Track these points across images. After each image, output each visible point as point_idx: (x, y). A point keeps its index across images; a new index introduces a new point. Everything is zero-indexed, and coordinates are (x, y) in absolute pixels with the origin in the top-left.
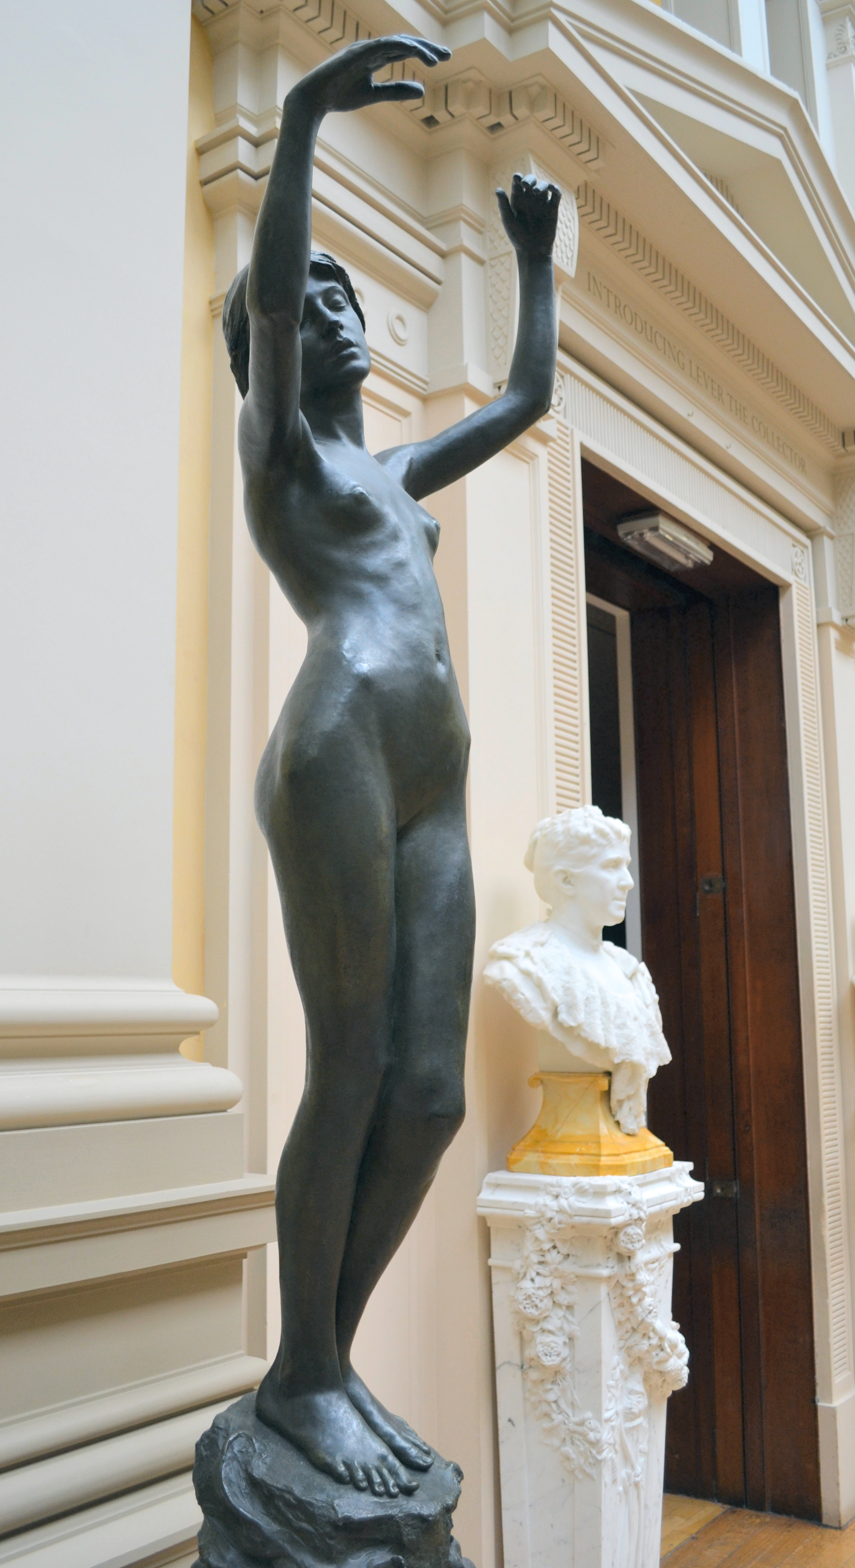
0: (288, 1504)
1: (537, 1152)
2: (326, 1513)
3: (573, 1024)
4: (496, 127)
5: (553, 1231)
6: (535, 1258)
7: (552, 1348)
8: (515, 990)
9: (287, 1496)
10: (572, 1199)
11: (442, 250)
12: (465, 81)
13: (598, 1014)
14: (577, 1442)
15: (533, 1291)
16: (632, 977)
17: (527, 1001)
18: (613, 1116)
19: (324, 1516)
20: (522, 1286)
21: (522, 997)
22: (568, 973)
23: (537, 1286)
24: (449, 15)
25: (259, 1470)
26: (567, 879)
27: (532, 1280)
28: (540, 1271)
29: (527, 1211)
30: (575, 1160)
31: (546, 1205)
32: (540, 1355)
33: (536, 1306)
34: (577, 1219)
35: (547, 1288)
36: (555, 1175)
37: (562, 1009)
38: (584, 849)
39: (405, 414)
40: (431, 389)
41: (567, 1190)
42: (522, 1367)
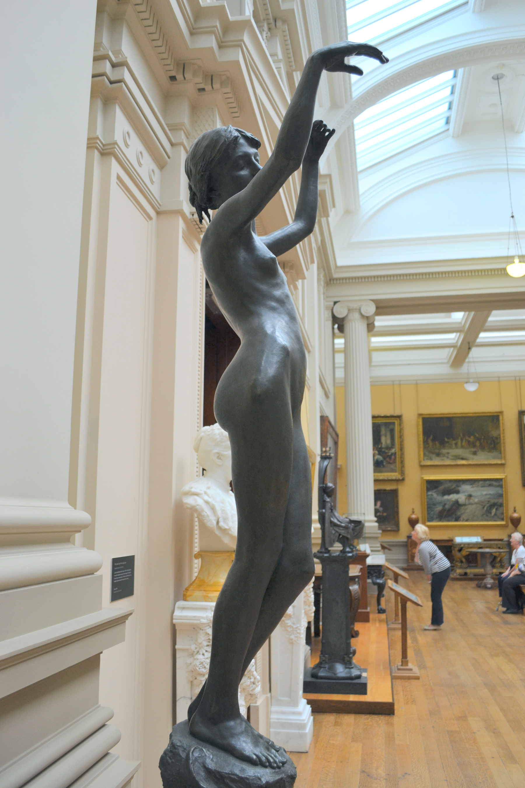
0: (233, 780)
2: (255, 782)
3: (227, 527)
8: (203, 510)
9: (232, 776)
12: (194, 64)
17: (208, 516)
19: (255, 784)
22: (223, 503)
24: (194, 31)
25: (211, 765)
27: (203, 654)
29: (202, 620)
33: (205, 667)
37: (221, 520)
39: (150, 218)
40: (162, 209)
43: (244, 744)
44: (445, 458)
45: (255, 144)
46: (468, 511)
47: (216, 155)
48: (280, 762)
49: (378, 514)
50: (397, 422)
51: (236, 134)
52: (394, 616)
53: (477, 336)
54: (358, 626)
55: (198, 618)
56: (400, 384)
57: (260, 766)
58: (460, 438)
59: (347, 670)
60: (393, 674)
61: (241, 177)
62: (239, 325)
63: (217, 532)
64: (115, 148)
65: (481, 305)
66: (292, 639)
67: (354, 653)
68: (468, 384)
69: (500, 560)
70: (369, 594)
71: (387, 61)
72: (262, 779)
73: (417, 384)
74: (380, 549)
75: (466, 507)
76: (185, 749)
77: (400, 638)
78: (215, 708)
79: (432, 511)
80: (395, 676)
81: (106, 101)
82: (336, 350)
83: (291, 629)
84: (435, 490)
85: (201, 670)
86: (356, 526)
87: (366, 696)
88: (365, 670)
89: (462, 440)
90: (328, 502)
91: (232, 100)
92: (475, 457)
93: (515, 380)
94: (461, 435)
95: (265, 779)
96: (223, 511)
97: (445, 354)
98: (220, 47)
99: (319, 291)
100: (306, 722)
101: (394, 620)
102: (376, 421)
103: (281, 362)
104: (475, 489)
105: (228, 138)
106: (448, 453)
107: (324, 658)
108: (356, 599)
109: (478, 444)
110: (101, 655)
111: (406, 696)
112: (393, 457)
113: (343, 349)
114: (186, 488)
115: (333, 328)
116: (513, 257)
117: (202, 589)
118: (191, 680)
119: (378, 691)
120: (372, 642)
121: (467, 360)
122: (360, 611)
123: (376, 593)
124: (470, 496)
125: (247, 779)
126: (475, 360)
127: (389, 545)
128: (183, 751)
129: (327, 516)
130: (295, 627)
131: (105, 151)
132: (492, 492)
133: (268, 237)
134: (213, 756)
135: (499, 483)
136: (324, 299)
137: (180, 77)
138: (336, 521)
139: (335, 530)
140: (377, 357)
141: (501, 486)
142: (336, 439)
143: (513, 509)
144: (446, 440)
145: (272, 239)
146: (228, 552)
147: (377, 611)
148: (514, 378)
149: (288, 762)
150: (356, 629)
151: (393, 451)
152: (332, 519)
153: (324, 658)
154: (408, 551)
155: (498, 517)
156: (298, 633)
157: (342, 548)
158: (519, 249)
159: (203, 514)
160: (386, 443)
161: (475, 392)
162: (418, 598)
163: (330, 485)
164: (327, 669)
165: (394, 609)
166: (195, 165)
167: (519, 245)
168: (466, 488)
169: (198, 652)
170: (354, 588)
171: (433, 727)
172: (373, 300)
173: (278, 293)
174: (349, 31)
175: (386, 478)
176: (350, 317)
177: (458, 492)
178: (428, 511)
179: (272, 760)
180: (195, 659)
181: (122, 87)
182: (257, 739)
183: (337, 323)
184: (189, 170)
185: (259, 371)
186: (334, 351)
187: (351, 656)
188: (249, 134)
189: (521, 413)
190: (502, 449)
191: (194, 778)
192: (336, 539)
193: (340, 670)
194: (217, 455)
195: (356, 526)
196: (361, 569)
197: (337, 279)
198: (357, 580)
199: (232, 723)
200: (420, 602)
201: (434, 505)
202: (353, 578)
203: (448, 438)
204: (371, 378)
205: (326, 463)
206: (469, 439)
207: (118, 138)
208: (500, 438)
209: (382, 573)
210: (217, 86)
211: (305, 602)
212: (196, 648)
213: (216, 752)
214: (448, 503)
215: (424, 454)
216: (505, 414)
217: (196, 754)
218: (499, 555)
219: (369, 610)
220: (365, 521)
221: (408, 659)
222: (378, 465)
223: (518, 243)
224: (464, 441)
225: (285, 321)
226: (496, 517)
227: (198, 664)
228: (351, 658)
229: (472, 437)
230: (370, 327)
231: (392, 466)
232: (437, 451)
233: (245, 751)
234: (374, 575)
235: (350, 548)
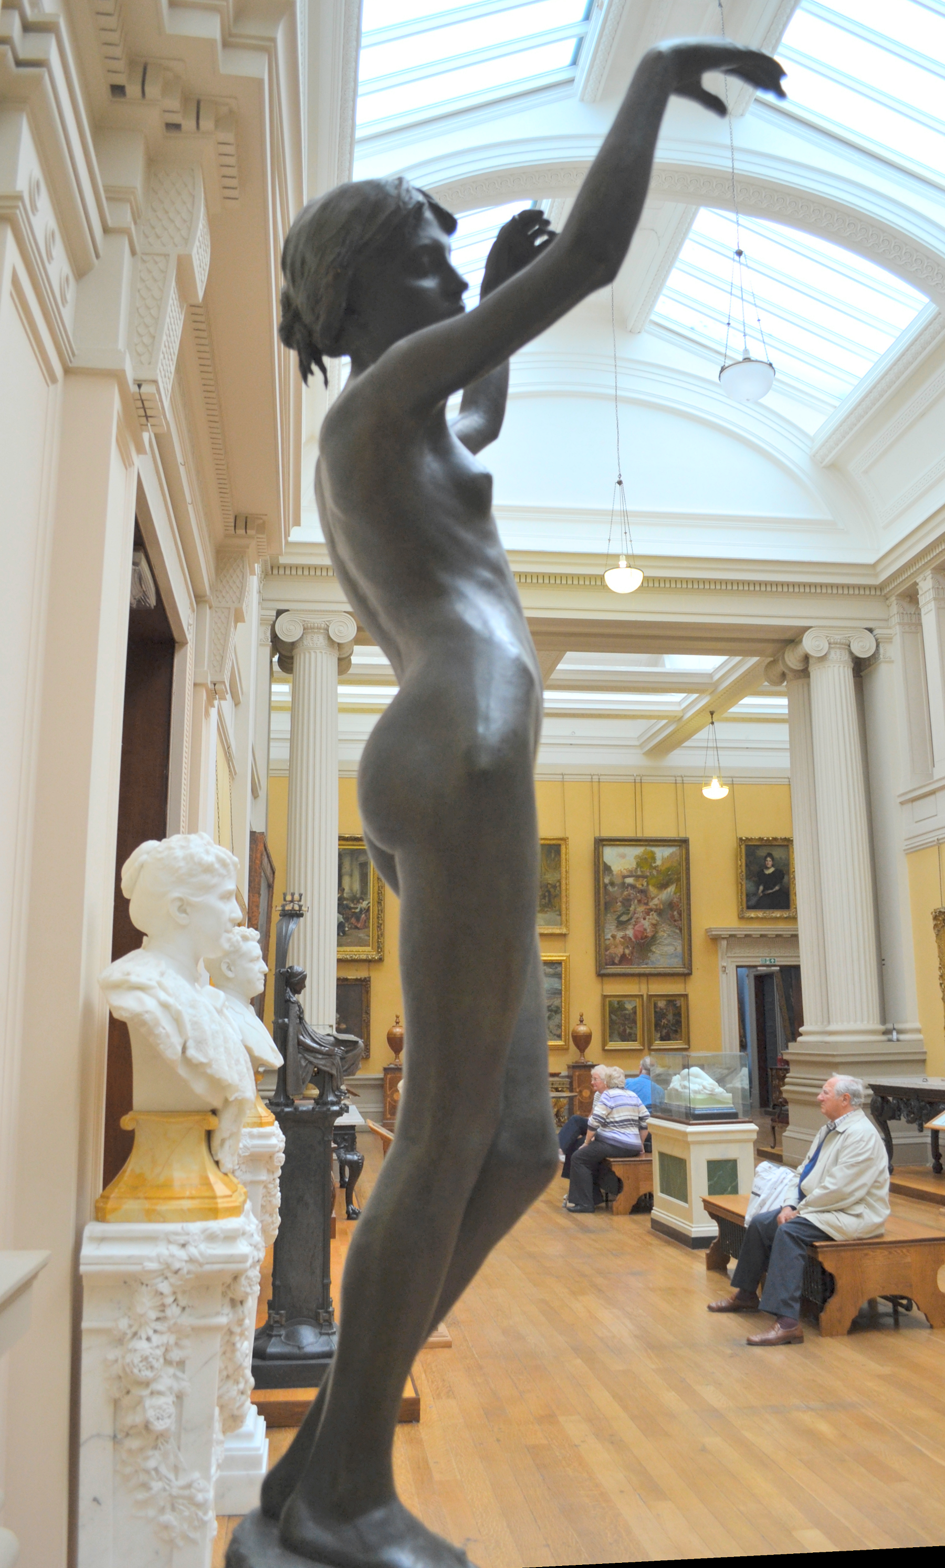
1: (139, 1198)
3: (203, 1060)
4: (174, 127)
5: (180, 1283)
6: (153, 1315)
7: (164, 1411)
8: (157, 1024)
10: (203, 1247)
13: (222, 1050)
14: (181, 1507)
17: (168, 1036)
18: (212, 1155)
21: (163, 1031)
26: (183, 906)
27: (148, 1339)
31: (173, 1256)
32: (152, 1419)
33: (152, 1367)
34: (208, 1267)
35: (162, 1345)
36: (164, 1222)
37: (190, 1044)
38: (206, 878)
39: (54, 380)
41: (196, 1237)
42: (115, 1437)
51: (421, 198)
55: (139, 1260)
59: (324, 1338)
61: (424, 291)
63: (182, 1071)
64: (17, 207)
85: (143, 1373)
86: (347, 1052)
96: (195, 1024)
98: (225, 45)
105: (404, 203)
107: (277, 1317)
115: (271, 662)
116: (617, 556)
118: (117, 1396)
129: (291, 1030)
137: (133, 90)
138: (308, 1041)
139: (306, 1059)
141: (559, 976)
146: (198, 1112)
147: (346, 1216)
151: (364, 904)
152: (301, 1037)
153: (277, 1317)
154: (385, 1096)
158: (629, 543)
159: (156, 1032)
160: (351, 889)
169: (135, 1334)
171: (498, 1440)
174: (361, 90)
176: (307, 642)
180: (130, 1351)
189: (601, 843)
190: (564, 906)
194: (178, 904)
195: (347, 1052)
208: (560, 886)
210: (207, 124)
211: (262, 1206)
212: (130, 1326)
216: (570, 842)
227: (136, 1361)
230: (344, 664)
231: (361, 935)
235: (336, 1096)
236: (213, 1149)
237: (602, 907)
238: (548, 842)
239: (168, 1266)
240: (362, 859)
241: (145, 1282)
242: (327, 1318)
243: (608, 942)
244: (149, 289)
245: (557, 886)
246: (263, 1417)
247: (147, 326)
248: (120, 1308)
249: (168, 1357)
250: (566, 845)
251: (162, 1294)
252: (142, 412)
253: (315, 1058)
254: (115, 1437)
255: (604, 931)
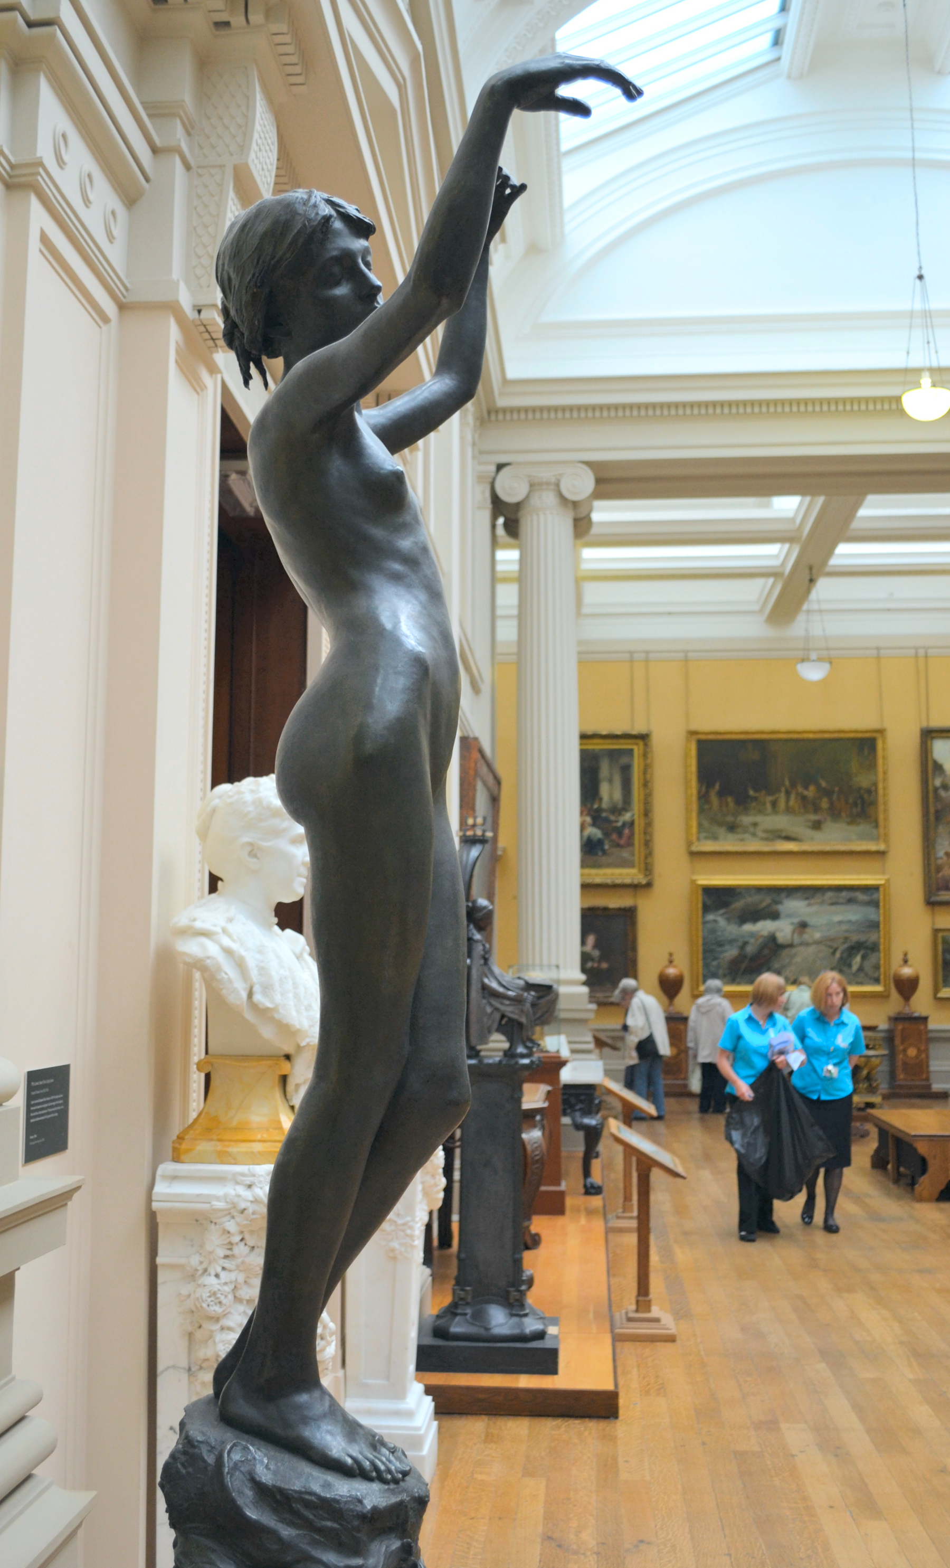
0: (308, 1504)
1: (212, 1140)
3: (269, 1005)
5: (246, 1222)
6: (221, 1252)
8: (219, 969)
9: (307, 1497)
11: (155, 144)
13: (291, 995)
15: (219, 1287)
16: (299, 957)
17: (230, 981)
18: (287, 1100)
19: (352, 1511)
20: (206, 1283)
21: (226, 976)
22: (260, 952)
23: (223, 1281)
25: (265, 1477)
26: (253, 851)
27: (217, 1276)
28: (226, 1265)
29: (214, 1203)
30: (258, 1147)
31: (239, 1196)
33: (220, 1303)
35: (231, 1282)
36: (235, 1164)
37: (257, 989)
39: (106, 319)
40: (130, 298)
41: (262, 1179)
42: (189, 1369)
43: (329, 1438)
44: (746, 836)
45: (363, 229)
46: (798, 959)
47: (284, 254)
48: (398, 1472)
49: (589, 965)
50: (637, 749)
51: (327, 210)
52: (621, 1200)
53: (830, 552)
54: (538, 1224)
55: (207, 1199)
56: (647, 661)
57: (359, 1479)
58: (783, 789)
60: (617, 1331)
61: (336, 299)
62: (326, 609)
63: (249, 1016)
64: (39, 174)
65: (840, 483)
66: (393, 1250)
67: (530, 1282)
68: (805, 665)
69: (869, 1074)
70: (565, 1151)
71: (640, 93)
72: (366, 1502)
73: (686, 660)
74: (591, 1046)
75: (794, 951)
76: (213, 1448)
77: (635, 1251)
78: (271, 1367)
79: (715, 959)
80: (620, 1335)
81: (16, 65)
82: (499, 575)
83: (393, 1228)
84: (722, 911)
85: (212, 1308)
86: (539, 998)
87: (556, 1377)
88: (555, 1321)
89: (788, 793)
90: (477, 941)
91: (290, 49)
92: (817, 835)
93: (916, 656)
94: (787, 783)
95: (371, 1501)
96: (262, 970)
97: (753, 592)
99: (462, 439)
100: (422, 1432)
101: (621, 1210)
102: (590, 747)
103: (412, 690)
104: (815, 908)
105: (309, 220)
106: (755, 825)
108: (537, 1161)
109: (825, 804)
110: (17, 1273)
111: (644, 1378)
112: (626, 831)
113: (516, 575)
114: (182, 920)
115: (494, 527)
116: (918, 371)
117: (215, 1137)
118: (190, 1329)
119: (582, 1366)
120: (570, 1260)
121: (805, 607)
122: (543, 1188)
123: (581, 1149)
124: (803, 925)
125: (337, 1501)
126: (824, 606)
127: (608, 1037)
128: (209, 1451)
129: (474, 973)
130: (400, 1222)
131: (16, 180)
132: (853, 918)
133: (381, 412)
134: (268, 1459)
135: (870, 895)
136: (474, 457)
138: (494, 985)
139: (491, 1005)
140: (594, 594)
142: (496, 792)
143: (901, 957)
144: (751, 793)
145: (390, 414)
146: (270, 1057)
148: (913, 651)
149: (412, 1474)
150: (534, 1229)
151: (627, 817)
152: (486, 981)
155: (866, 975)
156: (407, 1235)
157: (506, 1045)
159: (219, 977)
160: (611, 798)
161: (823, 682)
162: (677, 1160)
163: (483, 902)
164: (468, 1317)
165: (621, 1185)
166: (241, 270)
167: (932, 344)
168: (795, 907)
169: (205, 1270)
170: (533, 1136)
171: (704, 1444)
172: (588, 464)
173: (405, 544)
175: (609, 881)
176: (535, 501)
177: (775, 916)
178: (704, 958)
179: (382, 1468)
180: (199, 1286)
181: (54, 35)
182: (352, 1429)
183: (502, 514)
184: (226, 277)
185: (368, 706)
186: (494, 579)
187: (523, 1288)
188: (352, 210)
189: (929, 735)
190: (881, 816)
191: (233, 1501)
192: (495, 1026)
193: (499, 1320)
195: (539, 998)
196: (549, 1092)
197: (504, 410)
198: (538, 1118)
199: (303, 1398)
200: (680, 1169)
201: (720, 944)
202: (530, 1115)
203: (756, 790)
204: (580, 643)
205: (475, 852)
206: (806, 793)
207: (44, 151)
208: (876, 791)
209: (597, 1102)
210: (256, 17)
212: (201, 1263)
213: (273, 1452)
214: (752, 941)
215: (700, 826)
216: (890, 735)
217: (237, 1456)
218: (866, 1064)
219: (563, 1186)
220: (559, 982)
221: (651, 1296)
222: (591, 850)
223: (931, 340)
224: (793, 796)
225: (421, 603)
226: (861, 976)
227: (205, 1296)
228: (523, 1294)
229: (812, 788)
230: (581, 526)
231: (625, 854)
232: (730, 819)
233: (331, 1450)
234: (578, 1107)
235: (526, 1047)
236: (288, 1094)
237: (932, 817)
238: (860, 735)
239: (234, 1206)
240: (624, 760)
241: (214, 1221)
242: (517, 1297)
243: (939, 862)
244: (206, 206)
245: (872, 791)
246: (430, 1398)
247: (205, 247)
248: (192, 1246)
249: (237, 1295)
250: (884, 739)
251: (229, 1232)
252: (207, 336)
253: (502, 1004)
254: (189, 1369)
255: (934, 848)
